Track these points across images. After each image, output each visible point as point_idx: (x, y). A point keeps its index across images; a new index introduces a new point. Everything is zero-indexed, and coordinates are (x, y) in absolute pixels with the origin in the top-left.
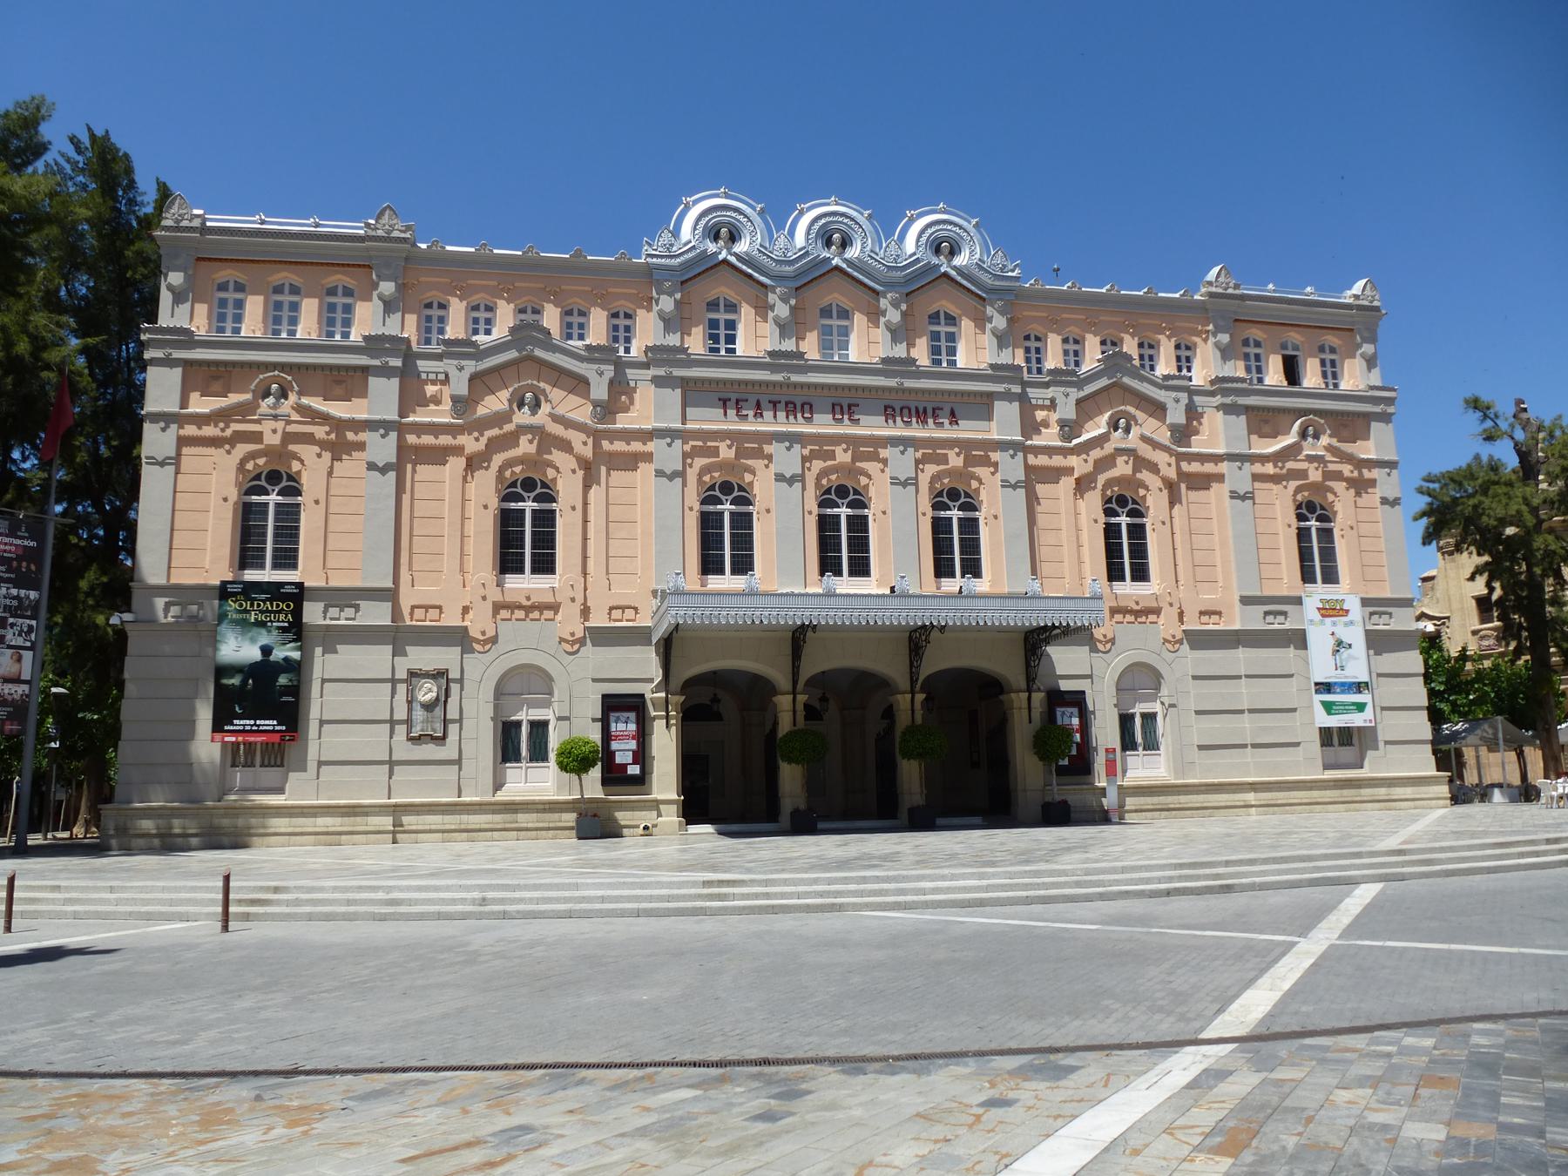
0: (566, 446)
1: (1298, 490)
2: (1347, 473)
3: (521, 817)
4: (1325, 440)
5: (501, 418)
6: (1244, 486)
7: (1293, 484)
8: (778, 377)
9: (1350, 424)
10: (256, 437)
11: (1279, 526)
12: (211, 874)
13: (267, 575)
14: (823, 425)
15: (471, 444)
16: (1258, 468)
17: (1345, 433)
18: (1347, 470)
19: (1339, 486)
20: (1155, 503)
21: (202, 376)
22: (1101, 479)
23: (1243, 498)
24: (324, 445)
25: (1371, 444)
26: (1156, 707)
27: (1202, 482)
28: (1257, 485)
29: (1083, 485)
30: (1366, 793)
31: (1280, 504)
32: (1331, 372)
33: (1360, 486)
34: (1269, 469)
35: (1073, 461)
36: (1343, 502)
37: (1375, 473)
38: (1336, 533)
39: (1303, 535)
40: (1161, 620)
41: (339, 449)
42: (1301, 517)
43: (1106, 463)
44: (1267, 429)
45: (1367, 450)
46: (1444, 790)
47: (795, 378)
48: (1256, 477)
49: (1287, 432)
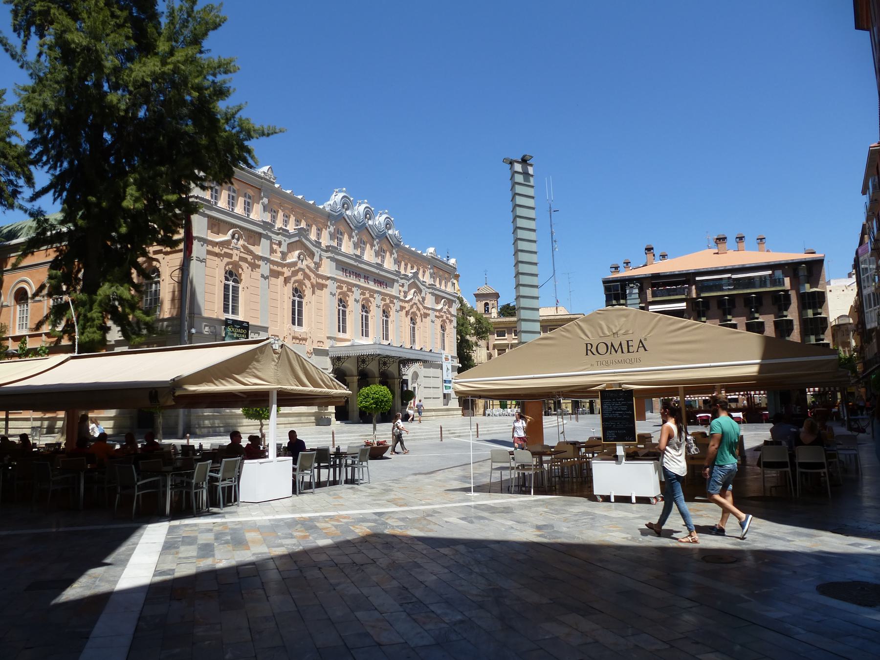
0: (309, 279)
1: (228, 264)
2: (249, 260)
3: (303, 418)
4: (241, 242)
5: (294, 264)
6: (267, 273)
7: (226, 260)
8: (355, 264)
9: (254, 237)
10: (230, 256)
11: (286, 298)
12: (327, 433)
13: (230, 316)
14: (372, 286)
15: (287, 272)
16: (210, 248)
17: (251, 241)
18: (249, 258)
19: (245, 265)
20: (308, 292)
21: (216, 225)
22: (293, 279)
23: (201, 261)
24: (249, 263)
25: (260, 248)
26: (416, 385)
27: (322, 287)
28: (209, 257)
29: (286, 281)
30: (452, 412)
31: (438, 322)
32: (248, 208)
33: (254, 266)
34: (216, 250)
35: (285, 270)
36: (246, 273)
37: (260, 263)
38: (240, 289)
39: (226, 287)
40: (307, 344)
41: (254, 266)
42: (227, 279)
43: (295, 273)
44: (215, 229)
45: (258, 250)
46: (460, 412)
47: (360, 265)
48: (209, 253)
49: (226, 234)
